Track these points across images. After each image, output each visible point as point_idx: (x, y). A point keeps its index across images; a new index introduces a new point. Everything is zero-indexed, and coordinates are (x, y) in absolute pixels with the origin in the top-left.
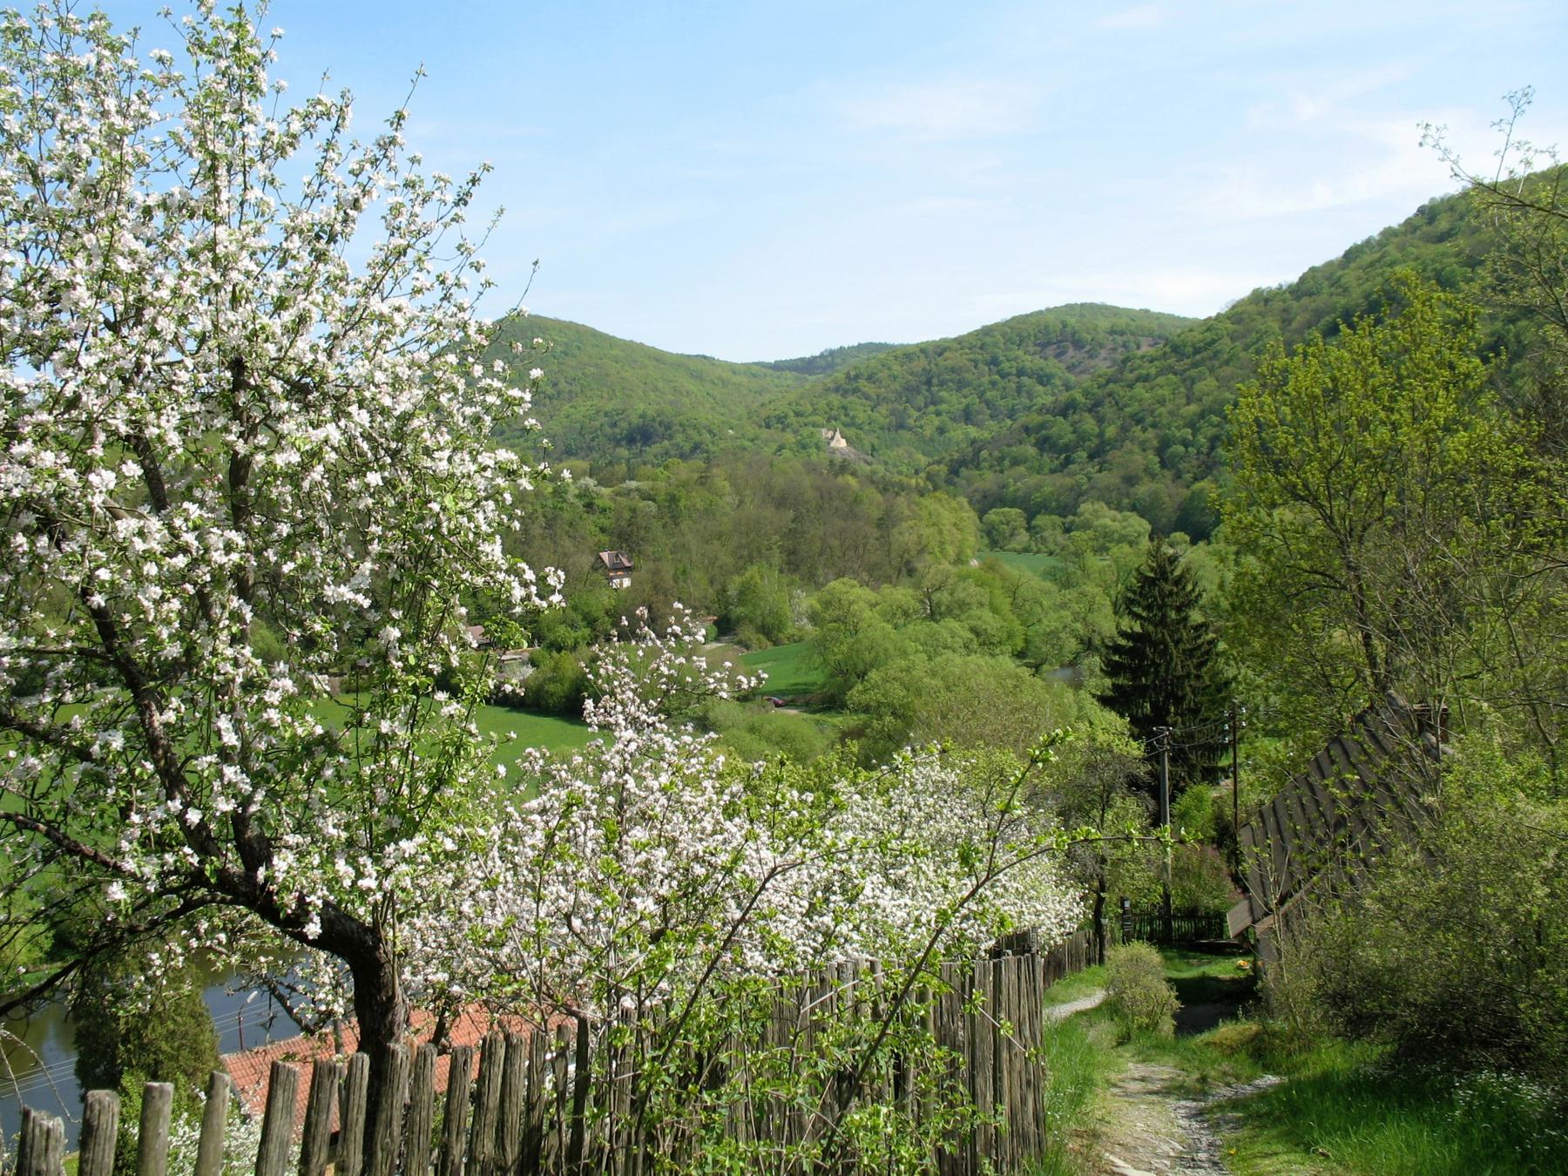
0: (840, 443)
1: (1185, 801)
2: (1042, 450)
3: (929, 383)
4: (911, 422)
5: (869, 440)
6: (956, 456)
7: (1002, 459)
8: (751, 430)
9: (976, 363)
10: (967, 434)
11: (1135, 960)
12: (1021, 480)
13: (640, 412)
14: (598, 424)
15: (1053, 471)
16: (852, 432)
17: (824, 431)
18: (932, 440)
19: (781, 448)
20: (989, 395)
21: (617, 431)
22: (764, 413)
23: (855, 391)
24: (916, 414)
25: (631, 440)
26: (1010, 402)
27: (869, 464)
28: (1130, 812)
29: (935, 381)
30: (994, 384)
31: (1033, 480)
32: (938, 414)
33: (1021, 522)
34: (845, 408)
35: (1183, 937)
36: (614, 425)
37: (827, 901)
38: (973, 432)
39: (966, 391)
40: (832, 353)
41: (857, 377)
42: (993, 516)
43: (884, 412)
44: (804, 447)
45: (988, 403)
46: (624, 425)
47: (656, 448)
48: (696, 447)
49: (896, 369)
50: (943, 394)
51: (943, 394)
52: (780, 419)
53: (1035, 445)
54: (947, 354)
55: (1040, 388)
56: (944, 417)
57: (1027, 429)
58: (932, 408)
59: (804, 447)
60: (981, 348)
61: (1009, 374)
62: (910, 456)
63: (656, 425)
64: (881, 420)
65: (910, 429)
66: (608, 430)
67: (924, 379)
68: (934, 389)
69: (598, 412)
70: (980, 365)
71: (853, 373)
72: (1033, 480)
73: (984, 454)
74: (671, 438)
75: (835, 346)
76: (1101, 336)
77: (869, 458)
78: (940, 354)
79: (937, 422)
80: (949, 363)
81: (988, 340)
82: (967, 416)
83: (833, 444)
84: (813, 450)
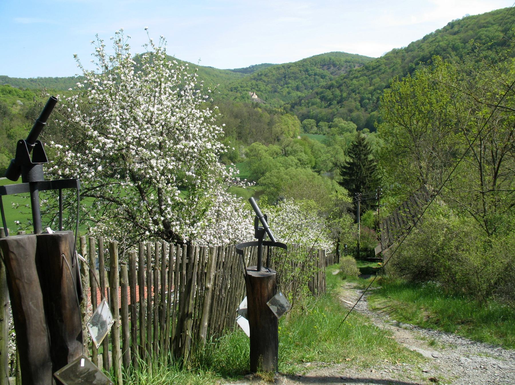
0: (255, 97)
1: (365, 215)
2: (322, 100)
3: (285, 77)
4: (279, 90)
5: (265, 96)
7: (309, 103)
8: (226, 92)
9: (301, 71)
10: (297, 94)
11: (348, 261)
12: (315, 110)
15: (325, 107)
16: (259, 93)
19: (236, 98)
20: (305, 81)
22: (230, 86)
23: (260, 79)
24: (280, 87)
26: (312, 84)
27: (265, 104)
28: (348, 219)
29: (287, 77)
30: (306, 78)
31: (319, 110)
32: (288, 87)
33: (315, 124)
34: (257, 85)
35: (363, 257)
38: (299, 94)
39: (297, 80)
40: (253, 67)
41: (261, 75)
42: (305, 122)
45: (304, 84)
50: (290, 81)
51: (290, 81)
54: (291, 68)
56: (290, 89)
57: (317, 93)
58: (286, 86)
59: (243, 98)
62: (278, 101)
67: (283, 76)
68: (287, 79)
71: (260, 74)
72: (319, 110)
73: (303, 101)
76: (342, 63)
77: (265, 102)
79: (287, 90)
80: (292, 71)
81: (305, 63)
82: (297, 89)
84: (246, 99)
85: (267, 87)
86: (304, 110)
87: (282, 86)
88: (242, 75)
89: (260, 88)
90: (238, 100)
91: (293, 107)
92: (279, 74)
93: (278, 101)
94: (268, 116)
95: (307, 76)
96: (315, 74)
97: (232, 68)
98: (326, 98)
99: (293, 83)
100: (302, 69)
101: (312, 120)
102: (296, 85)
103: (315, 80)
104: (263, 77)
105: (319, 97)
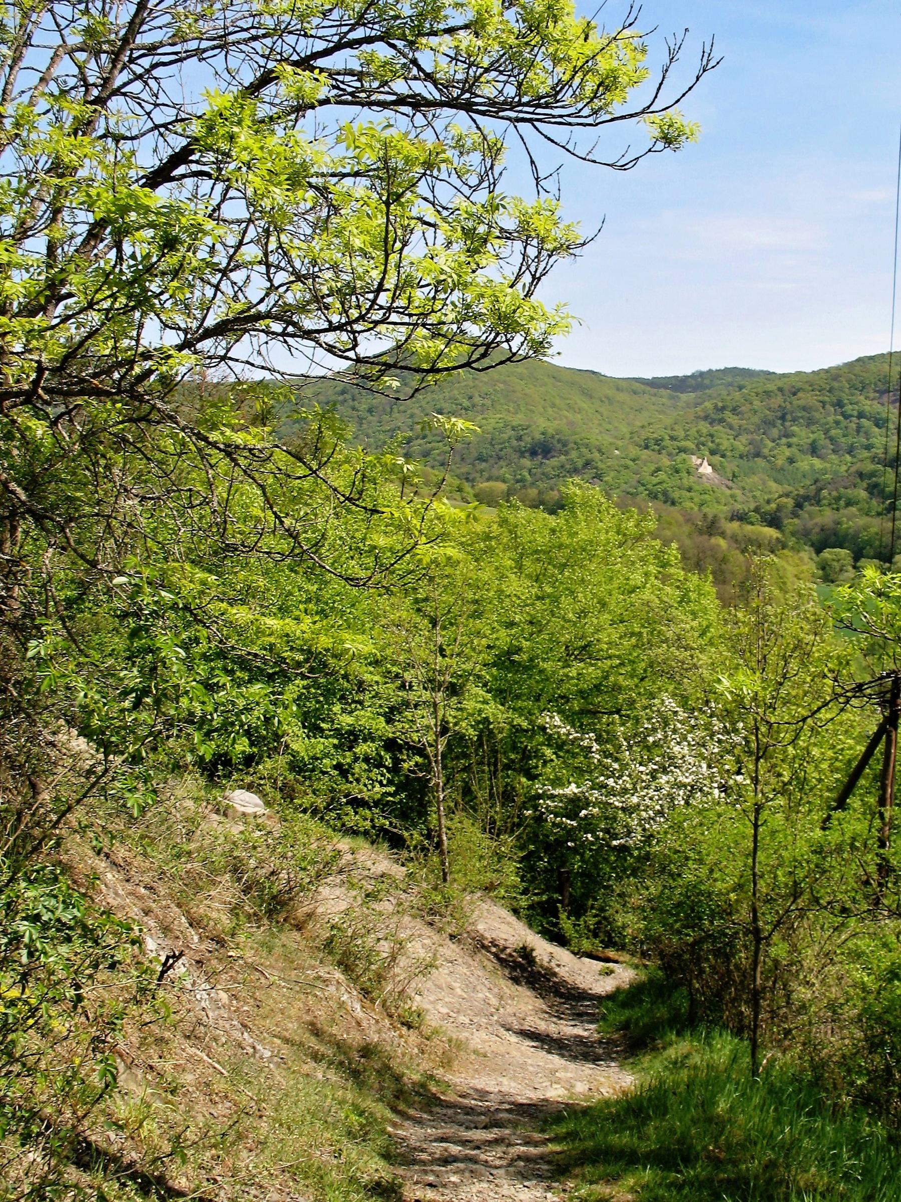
2: (871, 493)
3: (783, 418)
4: (766, 451)
5: (731, 466)
6: (802, 492)
7: (838, 499)
8: (634, 451)
9: (824, 403)
10: (812, 465)
12: (854, 521)
13: (541, 429)
14: (506, 436)
15: (879, 514)
16: (717, 459)
17: (694, 458)
18: (782, 469)
19: (658, 470)
20: (833, 432)
21: (523, 444)
22: (644, 434)
23: (722, 421)
24: (771, 445)
25: (533, 453)
26: (850, 440)
27: (730, 488)
29: (789, 417)
30: (837, 423)
31: (862, 521)
32: (789, 446)
33: (849, 561)
34: (712, 436)
36: (519, 439)
37: (566, 520)
39: (814, 428)
40: (701, 374)
41: (723, 408)
42: (827, 554)
43: (744, 441)
44: (677, 472)
45: (831, 439)
46: (529, 439)
47: (554, 462)
48: (587, 464)
49: (757, 403)
50: (794, 428)
51: (794, 428)
52: (658, 442)
53: (866, 490)
54: (800, 394)
55: (876, 429)
56: (794, 449)
57: (861, 475)
58: (784, 440)
59: (677, 472)
60: (829, 391)
61: (852, 416)
62: (764, 484)
63: (555, 442)
64: (742, 448)
65: (765, 457)
66: (515, 443)
67: (779, 414)
68: (788, 424)
69: (506, 426)
70: (828, 406)
71: (720, 404)
72: (862, 521)
73: (825, 492)
74: (566, 453)
75: (705, 369)
77: (730, 484)
78: (794, 394)
79: (788, 452)
80: (802, 403)
81: (835, 384)
82: (814, 450)
83: (701, 470)
84: (684, 474)
85: (736, 443)
86: (825, 517)
87: (773, 441)
88: (671, 398)
89: (718, 445)
90: (662, 476)
91: (799, 506)
92: (769, 409)
93: (764, 484)
94: (741, 558)
95: (840, 418)
96: (861, 415)
97: (648, 375)
98: (883, 491)
99: (803, 434)
100: (826, 399)
101: (844, 552)
102: (809, 441)
103: (858, 431)
104: (727, 414)
105: (865, 485)
